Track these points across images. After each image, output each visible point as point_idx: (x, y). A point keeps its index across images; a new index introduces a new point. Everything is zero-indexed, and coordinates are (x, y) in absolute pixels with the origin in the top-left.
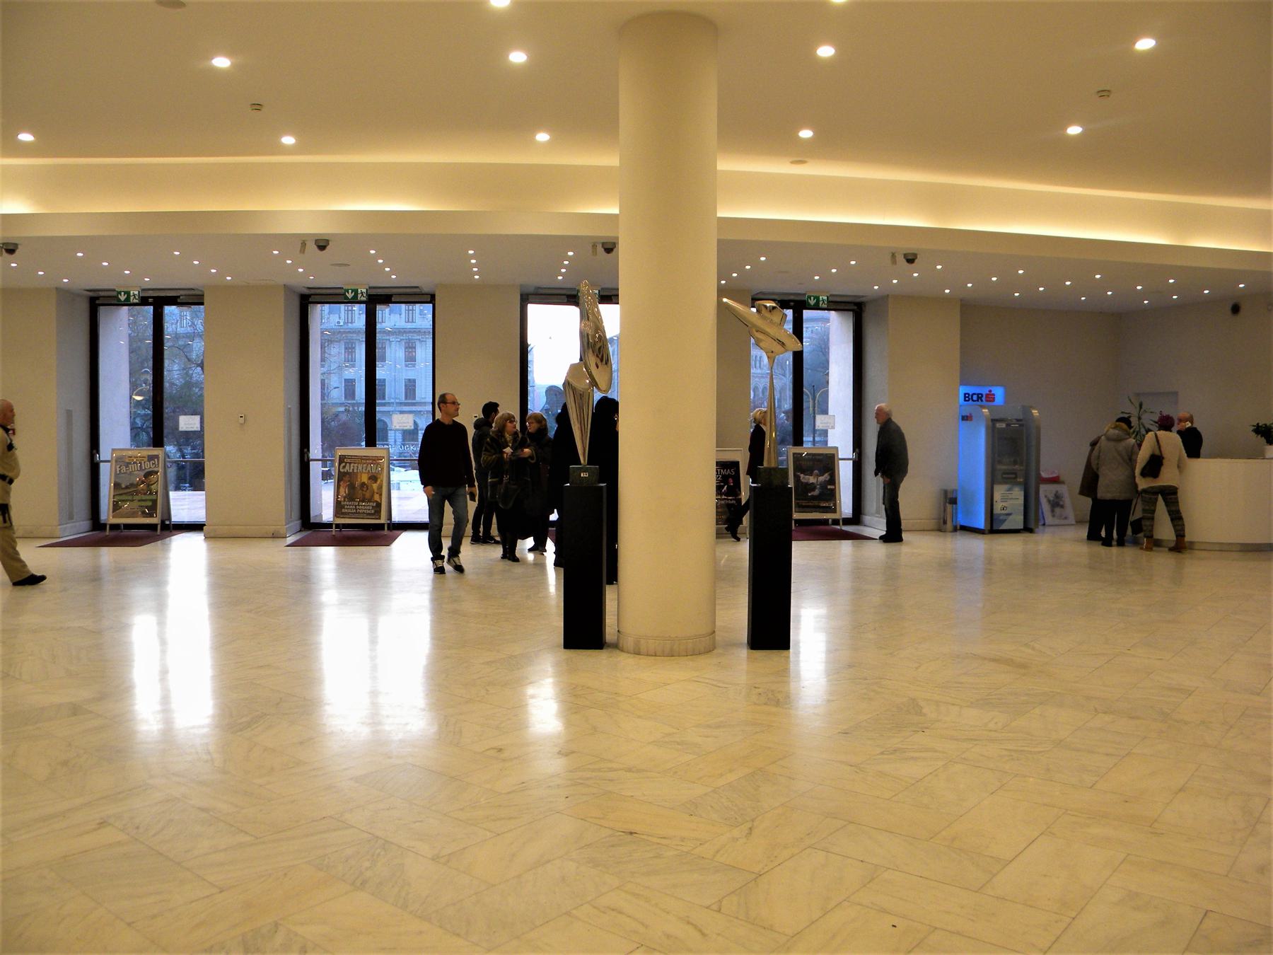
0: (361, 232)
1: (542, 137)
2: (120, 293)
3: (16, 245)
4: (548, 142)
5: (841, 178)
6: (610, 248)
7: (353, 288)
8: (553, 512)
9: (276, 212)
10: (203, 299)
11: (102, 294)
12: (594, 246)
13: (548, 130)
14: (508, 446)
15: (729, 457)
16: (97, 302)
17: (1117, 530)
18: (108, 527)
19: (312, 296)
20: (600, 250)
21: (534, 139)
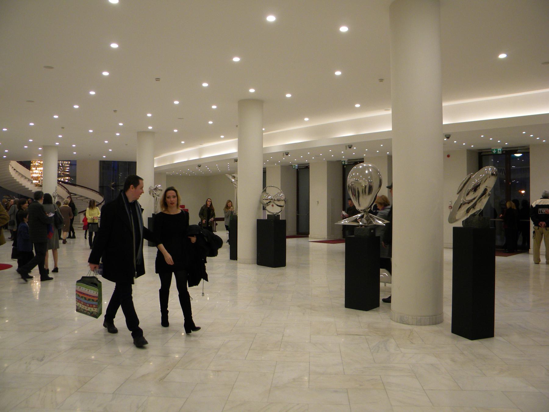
0: (332, 144)
1: (306, 119)
2: (342, 161)
3: (201, 165)
4: (224, 138)
5: (318, 126)
6: (236, 161)
7: (495, 149)
8: (190, 239)
9: (268, 147)
10: (529, 150)
11: (519, 148)
12: (346, 147)
13: (308, 117)
14: (44, 203)
15: (301, 241)
16: (482, 154)
17: (133, 264)
18: (389, 258)
19: (519, 150)
20: (348, 148)
21: (304, 119)
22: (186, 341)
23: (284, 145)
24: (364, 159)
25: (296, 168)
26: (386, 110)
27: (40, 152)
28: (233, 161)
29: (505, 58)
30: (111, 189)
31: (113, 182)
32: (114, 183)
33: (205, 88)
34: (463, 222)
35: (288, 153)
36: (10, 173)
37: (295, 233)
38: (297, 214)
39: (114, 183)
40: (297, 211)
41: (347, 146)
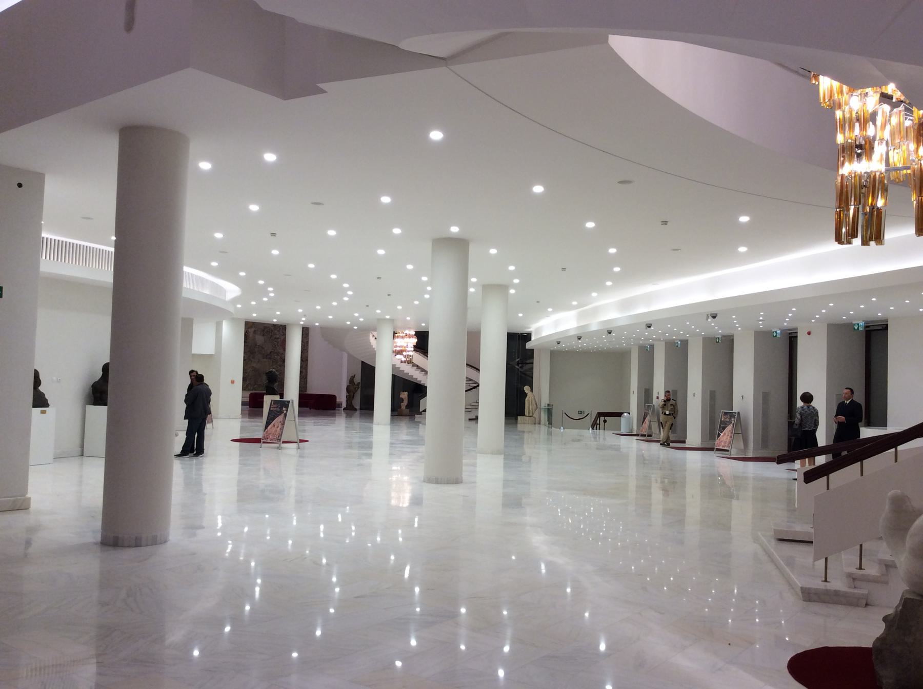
2: (855, 324)
22: (346, 427)
23: (630, 316)
24: (798, 333)
25: (861, 329)
26: (654, 284)
27: (427, 283)
28: (606, 332)
29: (742, 216)
30: (515, 367)
31: (518, 358)
32: (519, 359)
33: (400, 305)
34: (251, 393)
35: (651, 324)
36: (372, 346)
37: (783, 450)
38: (789, 420)
39: (519, 359)
40: (788, 413)
41: (709, 315)
